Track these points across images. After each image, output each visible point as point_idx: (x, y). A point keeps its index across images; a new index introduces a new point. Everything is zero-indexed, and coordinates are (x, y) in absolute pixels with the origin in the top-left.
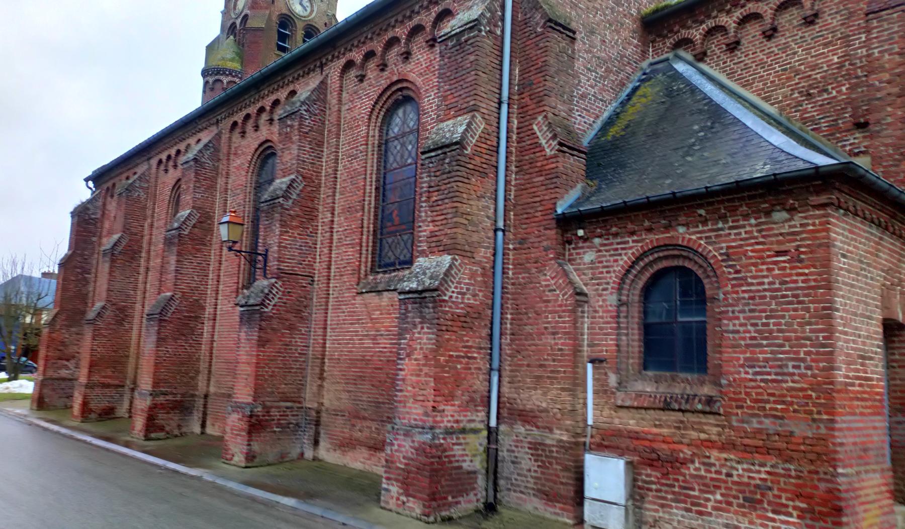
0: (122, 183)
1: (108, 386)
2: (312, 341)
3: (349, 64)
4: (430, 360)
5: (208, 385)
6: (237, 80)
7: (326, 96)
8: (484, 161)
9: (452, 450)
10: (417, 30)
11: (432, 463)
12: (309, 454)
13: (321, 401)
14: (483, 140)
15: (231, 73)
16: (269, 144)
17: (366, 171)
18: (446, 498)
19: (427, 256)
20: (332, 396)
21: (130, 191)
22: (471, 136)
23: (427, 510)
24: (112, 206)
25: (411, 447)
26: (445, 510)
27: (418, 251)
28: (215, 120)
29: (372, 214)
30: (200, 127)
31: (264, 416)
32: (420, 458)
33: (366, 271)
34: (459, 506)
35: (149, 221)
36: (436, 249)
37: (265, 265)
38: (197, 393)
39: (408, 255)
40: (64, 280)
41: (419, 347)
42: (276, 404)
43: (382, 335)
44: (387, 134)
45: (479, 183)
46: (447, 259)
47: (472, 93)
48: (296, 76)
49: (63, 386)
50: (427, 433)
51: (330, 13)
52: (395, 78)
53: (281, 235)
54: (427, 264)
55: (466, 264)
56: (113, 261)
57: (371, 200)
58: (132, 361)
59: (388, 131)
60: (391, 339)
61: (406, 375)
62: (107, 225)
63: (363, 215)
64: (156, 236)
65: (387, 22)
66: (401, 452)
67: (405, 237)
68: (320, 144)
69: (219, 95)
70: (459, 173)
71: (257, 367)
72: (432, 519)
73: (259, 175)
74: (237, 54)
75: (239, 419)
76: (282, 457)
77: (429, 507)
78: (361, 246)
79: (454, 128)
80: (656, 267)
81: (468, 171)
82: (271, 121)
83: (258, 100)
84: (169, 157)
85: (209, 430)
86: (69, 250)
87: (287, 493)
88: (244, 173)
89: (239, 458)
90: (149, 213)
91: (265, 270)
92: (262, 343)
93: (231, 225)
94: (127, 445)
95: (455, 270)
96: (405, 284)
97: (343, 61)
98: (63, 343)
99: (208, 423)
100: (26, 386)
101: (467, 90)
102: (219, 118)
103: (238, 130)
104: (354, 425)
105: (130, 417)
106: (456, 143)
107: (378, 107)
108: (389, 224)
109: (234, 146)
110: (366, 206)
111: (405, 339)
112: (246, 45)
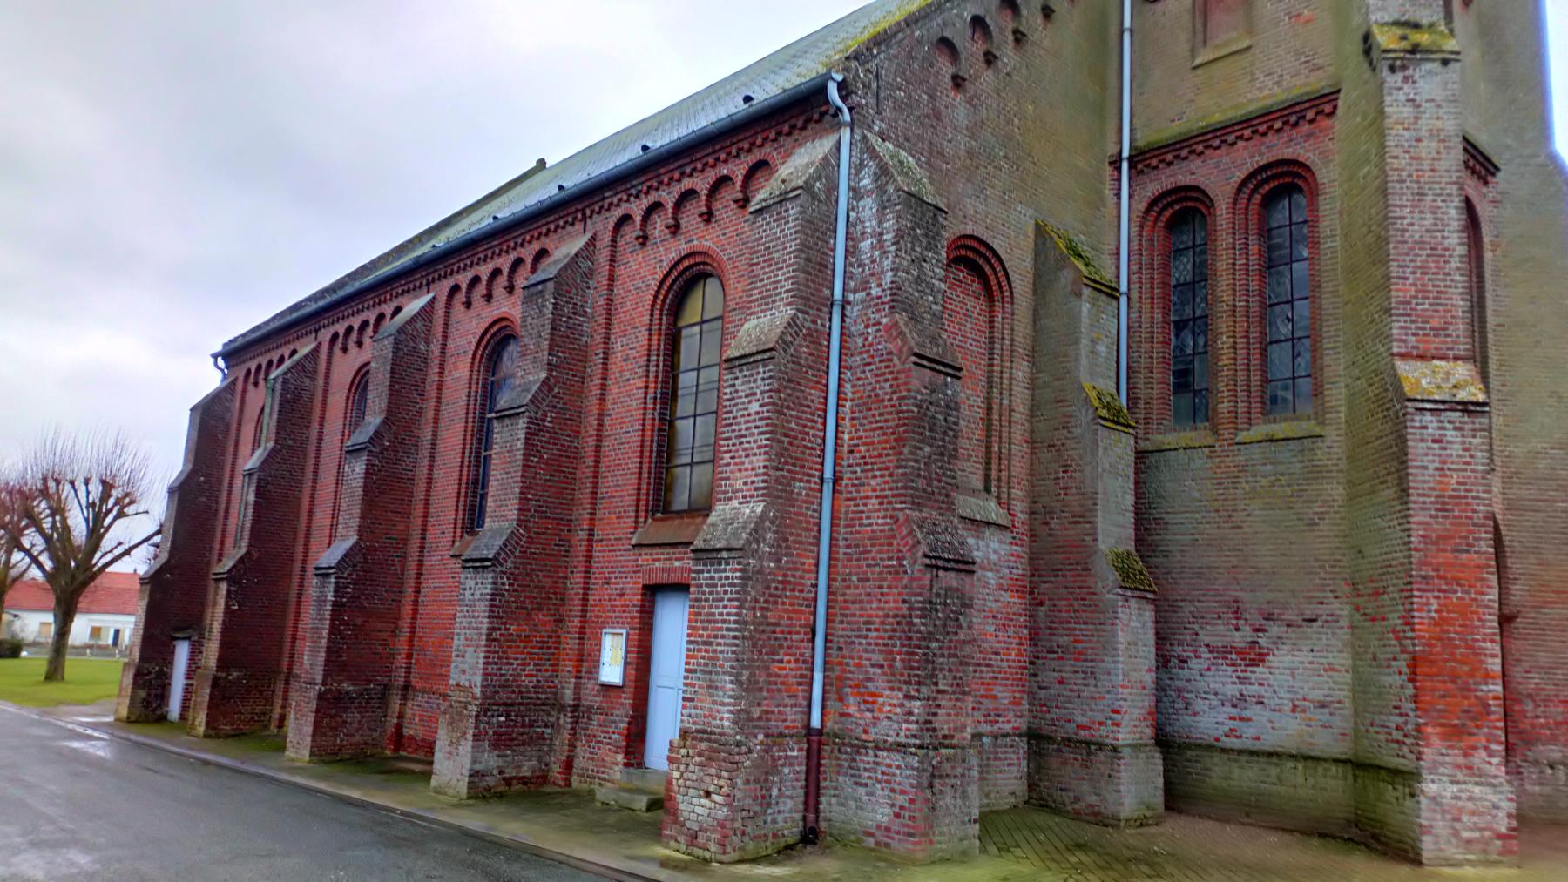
80: (971, 255)
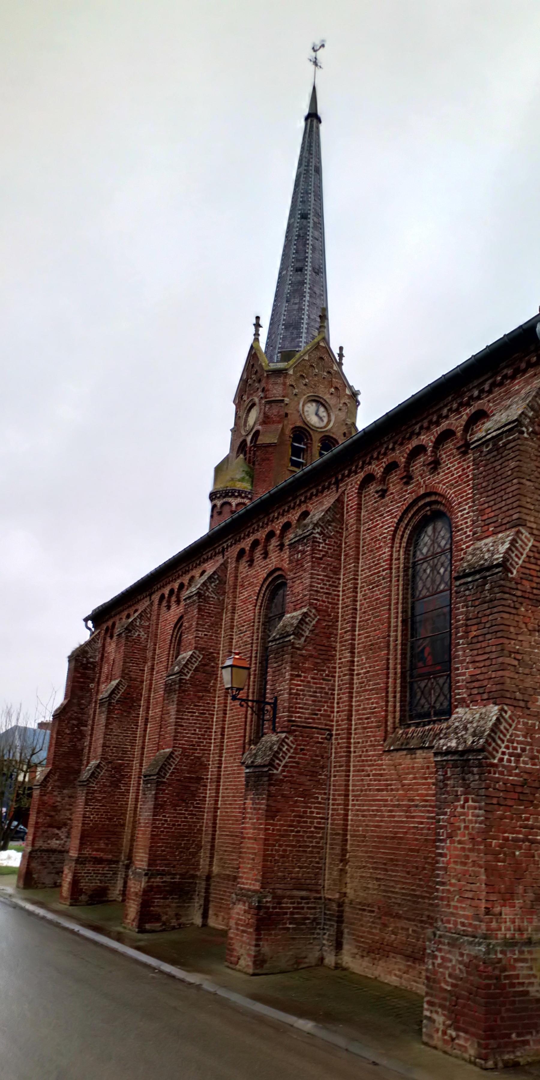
0: (121, 623)
1: (99, 861)
2: (330, 812)
3: (369, 478)
4: (479, 843)
5: (211, 865)
6: (246, 501)
7: (342, 515)
8: (535, 585)
9: (514, 968)
10: (448, 434)
11: (488, 986)
12: (330, 959)
13: (344, 890)
14: (533, 560)
15: (240, 494)
16: (280, 573)
17: (390, 600)
18: (509, 1036)
19: (468, 706)
20: (357, 885)
21: (130, 631)
22: (516, 555)
23: (484, 1051)
24: (111, 647)
25: (460, 962)
26: (509, 1052)
27: (456, 700)
28: (220, 548)
29: (399, 652)
30: (205, 557)
31: (274, 908)
32: (472, 978)
33: (394, 723)
34: (527, 1047)
35: (149, 664)
36: (478, 698)
37: (274, 717)
38: (198, 873)
39: (446, 704)
40: (58, 733)
41: (463, 825)
42: (288, 893)
43: (416, 806)
44: (414, 555)
45: (529, 614)
46: (494, 710)
47: (515, 505)
48: (309, 494)
49: (53, 859)
50: (480, 944)
51: (349, 422)
52: (422, 491)
53: (291, 680)
54: (468, 716)
55: (520, 717)
56: (109, 712)
57: (397, 635)
58: (128, 830)
59: (415, 552)
60: (428, 812)
61: (448, 863)
62: (105, 669)
63: (388, 654)
64: (158, 678)
65: (410, 430)
66: (447, 968)
67: (441, 681)
68: (336, 571)
69: (227, 518)
70: (503, 602)
71: (265, 845)
72: (490, 1064)
73: (268, 608)
74: (247, 473)
75: (245, 911)
76: (298, 963)
77: (486, 1046)
78: (387, 692)
79: (496, 547)
81: (515, 599)
82: (281, 547)
83: (267, 524)
84: (172, 591)
85: (212, 922)
86: (65, 698)
87: (302, 1014)
88: (251, 607)
89: (246, 962)
90: (149, 654)
91: (274, 723)
92: (271, 813)
93: (234, 669)
94: (119, 938)
95: (504, 724)
96: (442, 741)
97: (361, 475)
98: (54, 808)
99: (211, 912)
100: (12, 858)
101: (509, 502)
102: (225, 545)
103: (245, 559)
104: (385, 925)
105: (123, 901)
106: (498, 566)
107: (403, 524)
108: (420, 664)
109: (240, 576)
110: (392, 644)
111: (445, 814)
112: (256, 463)
